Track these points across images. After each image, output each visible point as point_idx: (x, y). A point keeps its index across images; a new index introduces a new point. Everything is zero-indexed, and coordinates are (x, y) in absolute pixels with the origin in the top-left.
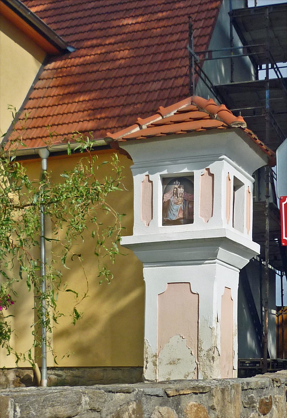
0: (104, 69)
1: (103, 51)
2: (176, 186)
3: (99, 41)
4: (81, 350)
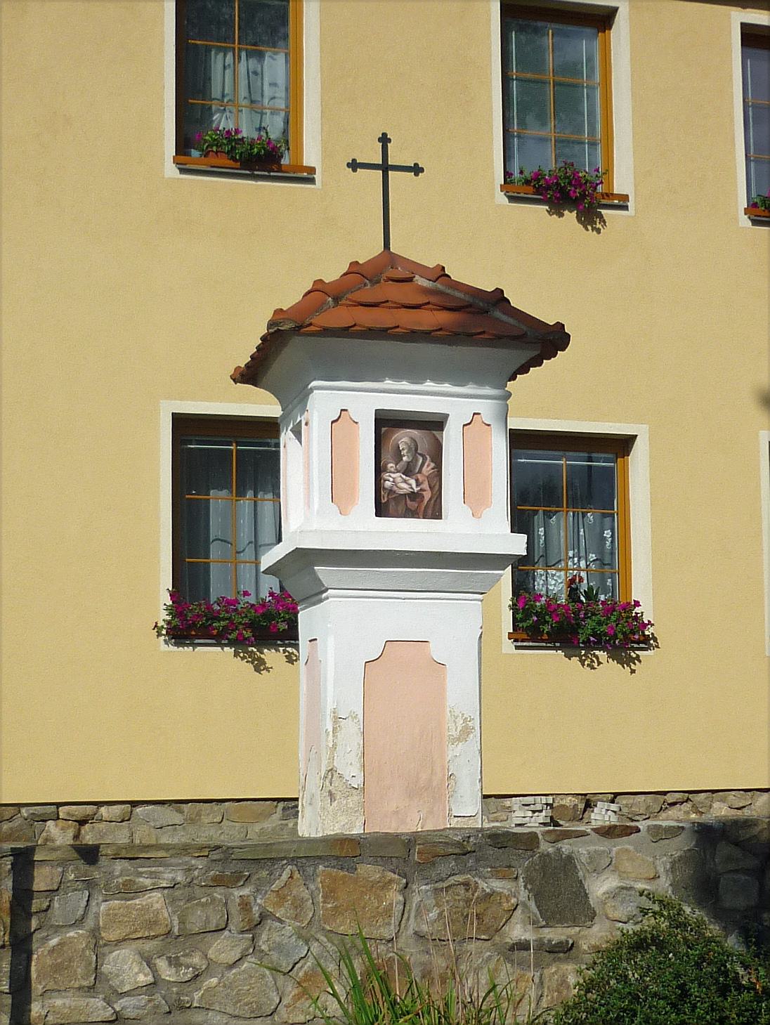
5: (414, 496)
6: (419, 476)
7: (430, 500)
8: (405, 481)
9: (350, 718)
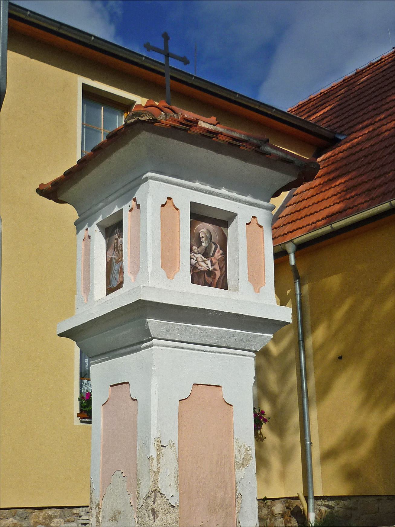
0: (367, 146)
1: (371, 129)
2: (117, 237)
3: (370, 121)
4: (351, 474)
5: (210, 273)
6: (213, 259)
7: (220, 278)
8: (204, 261)
9: (169, 446)
